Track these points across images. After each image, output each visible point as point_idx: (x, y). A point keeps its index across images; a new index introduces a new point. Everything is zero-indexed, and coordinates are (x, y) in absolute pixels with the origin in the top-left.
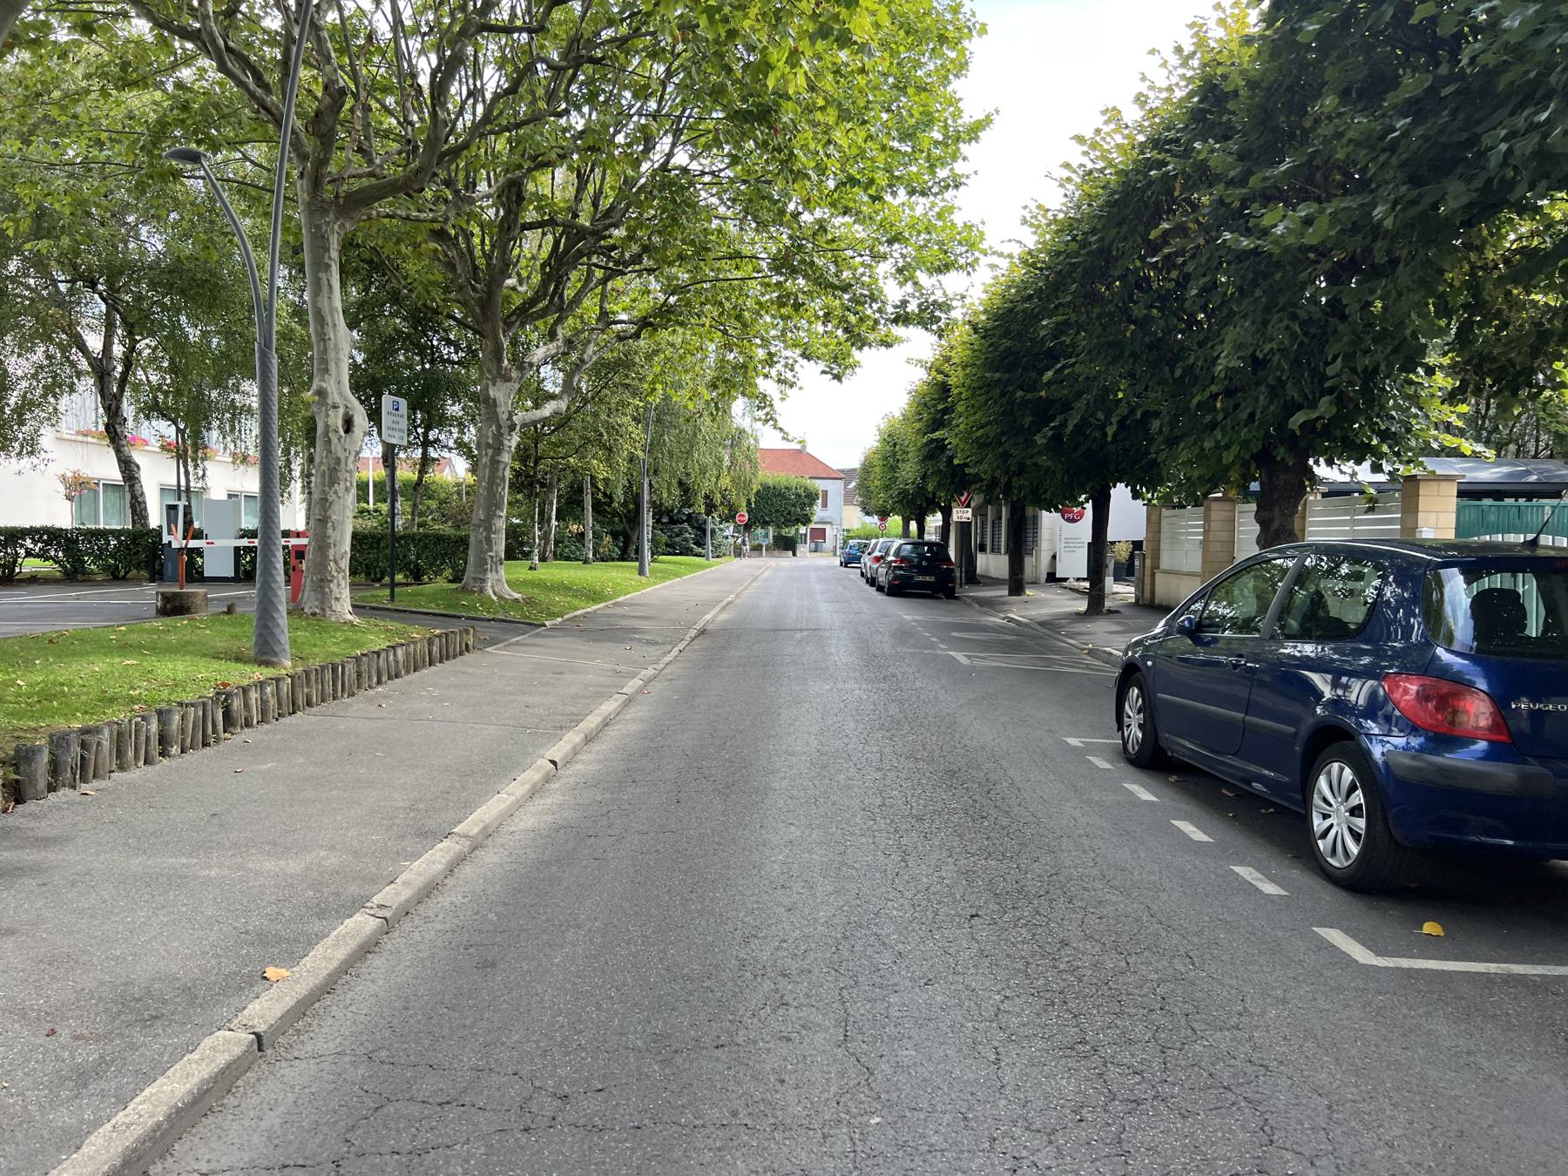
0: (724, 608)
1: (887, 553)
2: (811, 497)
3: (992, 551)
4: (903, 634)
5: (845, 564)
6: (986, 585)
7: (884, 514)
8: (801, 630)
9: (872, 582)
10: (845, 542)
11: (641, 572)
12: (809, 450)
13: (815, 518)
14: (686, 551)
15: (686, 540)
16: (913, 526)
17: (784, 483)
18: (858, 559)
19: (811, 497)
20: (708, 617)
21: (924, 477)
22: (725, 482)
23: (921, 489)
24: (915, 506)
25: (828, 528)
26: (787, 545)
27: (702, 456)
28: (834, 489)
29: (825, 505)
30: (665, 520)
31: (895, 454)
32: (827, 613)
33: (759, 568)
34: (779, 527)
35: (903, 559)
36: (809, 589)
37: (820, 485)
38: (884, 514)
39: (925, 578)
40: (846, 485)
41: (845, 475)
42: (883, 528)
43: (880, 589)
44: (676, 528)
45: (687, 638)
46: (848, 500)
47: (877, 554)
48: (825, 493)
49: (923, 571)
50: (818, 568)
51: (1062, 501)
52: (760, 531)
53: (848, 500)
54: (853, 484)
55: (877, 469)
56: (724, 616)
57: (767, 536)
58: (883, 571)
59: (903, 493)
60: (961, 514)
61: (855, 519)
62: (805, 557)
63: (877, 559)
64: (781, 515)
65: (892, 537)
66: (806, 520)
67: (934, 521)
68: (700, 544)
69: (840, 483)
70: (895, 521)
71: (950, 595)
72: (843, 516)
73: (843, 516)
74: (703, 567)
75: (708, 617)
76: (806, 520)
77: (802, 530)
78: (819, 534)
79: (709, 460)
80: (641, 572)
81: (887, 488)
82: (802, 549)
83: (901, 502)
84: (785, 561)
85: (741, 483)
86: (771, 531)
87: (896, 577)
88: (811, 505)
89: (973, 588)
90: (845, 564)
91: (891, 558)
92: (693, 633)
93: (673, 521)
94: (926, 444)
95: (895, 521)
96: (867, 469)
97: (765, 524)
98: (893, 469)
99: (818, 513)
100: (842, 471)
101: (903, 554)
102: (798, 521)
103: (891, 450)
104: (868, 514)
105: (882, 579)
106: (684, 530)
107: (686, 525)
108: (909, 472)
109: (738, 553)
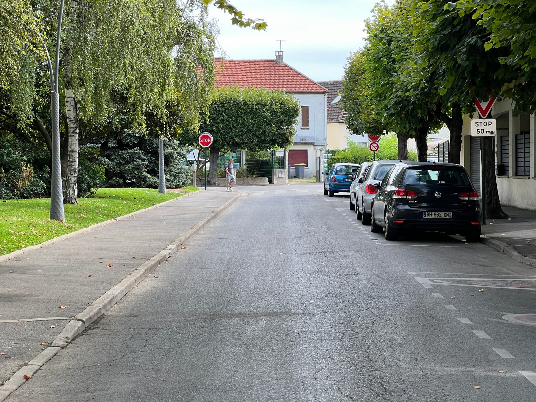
0: (151, 269)
1: (385, 181)
2: (289, 114)
3: (516, 174)
4: (426, 321)
5: (330, 193)
6: (515, 219)
7: (375, 132)
8: (257, 315)
9: (366, 218)
10: (330, 166)
11: (54, 215)
12: (286, 60)
13: (294, 139)
14: (140, 183)
15: (138, 168)
16: (412, 144)
17: (256, 98)
18: (347, 187)
19: (289, 114)
20: (115, 290)
21: (432, 78)
22: (172, 93)
23: (427, 95)
24: (414, 120)
25: (310, 149)
26: (262, 170)
27: (135, 57)
28: (317, 105)
29: (305, 123)
30: (112, 144)
31: (389, 54)
32: (303, 280)
33: (226, 199)
34: (251, 149)
35: (409, 190)
36: (280, 238)
37: (300, 100)
38: (375, 132)
39: (441, 215)
40: (330, 99)
41: (327, 89)
42: (375, 148)
43: (377, 229)
44: (126, 154)
45: (59, 341)
46: (332, 118)
47: (370, 181)
48: (306, 109)
49: (436, 205)
50: (299, 199)
51: (417, 134)
52: (230, 155)
53: (332, 118)
54: (338, 98)
55: (367, 75)
56: (148, 285)
57: (238, 160)
58: (380, 204)
59: (403, 102)
60: (479, 127)
61: (341, 138)
62: (283, 186)
63: (372, 189)
64: (250, 133)
65: (390, 160)
66: (284, 141)
67: (439, 137)
68: (154, 172)
69: (322, 99)
70: (389, 140)
71: (474, 237)
72: (327, 135)
73: (327, 135)
74: (151, 201)
75: (115, 290)
76: (284, 141)
77: (280, 152)
78: (299, 157)
79: (145, 63)
80: (54, 215)
81: (380, 96)
82: (280, 175)
83: (399, 113)
84: (259, 192)
85: (194, 94)
86: (244, 155)
87: (399, 215)
88: (289, 123)
89: (502, 224)
90: (330, 193)
91: (390, 188)
92: (74, 326)
93: (122, 146)
94: (436, 32)
95: (389, 140)
96: (354, 74)
97: (235, 147)
98: (388, 72)
99: (298, 131)
100: (325, 84)
101: (408, 181)
102: (274, 142)
103: (386, 46)
104: (356, 131)
105: (379, 217)
106: (125, 154)
107: (137, 150)
108: (411, 71)
109: (205, 180)
